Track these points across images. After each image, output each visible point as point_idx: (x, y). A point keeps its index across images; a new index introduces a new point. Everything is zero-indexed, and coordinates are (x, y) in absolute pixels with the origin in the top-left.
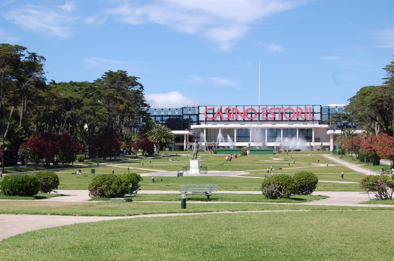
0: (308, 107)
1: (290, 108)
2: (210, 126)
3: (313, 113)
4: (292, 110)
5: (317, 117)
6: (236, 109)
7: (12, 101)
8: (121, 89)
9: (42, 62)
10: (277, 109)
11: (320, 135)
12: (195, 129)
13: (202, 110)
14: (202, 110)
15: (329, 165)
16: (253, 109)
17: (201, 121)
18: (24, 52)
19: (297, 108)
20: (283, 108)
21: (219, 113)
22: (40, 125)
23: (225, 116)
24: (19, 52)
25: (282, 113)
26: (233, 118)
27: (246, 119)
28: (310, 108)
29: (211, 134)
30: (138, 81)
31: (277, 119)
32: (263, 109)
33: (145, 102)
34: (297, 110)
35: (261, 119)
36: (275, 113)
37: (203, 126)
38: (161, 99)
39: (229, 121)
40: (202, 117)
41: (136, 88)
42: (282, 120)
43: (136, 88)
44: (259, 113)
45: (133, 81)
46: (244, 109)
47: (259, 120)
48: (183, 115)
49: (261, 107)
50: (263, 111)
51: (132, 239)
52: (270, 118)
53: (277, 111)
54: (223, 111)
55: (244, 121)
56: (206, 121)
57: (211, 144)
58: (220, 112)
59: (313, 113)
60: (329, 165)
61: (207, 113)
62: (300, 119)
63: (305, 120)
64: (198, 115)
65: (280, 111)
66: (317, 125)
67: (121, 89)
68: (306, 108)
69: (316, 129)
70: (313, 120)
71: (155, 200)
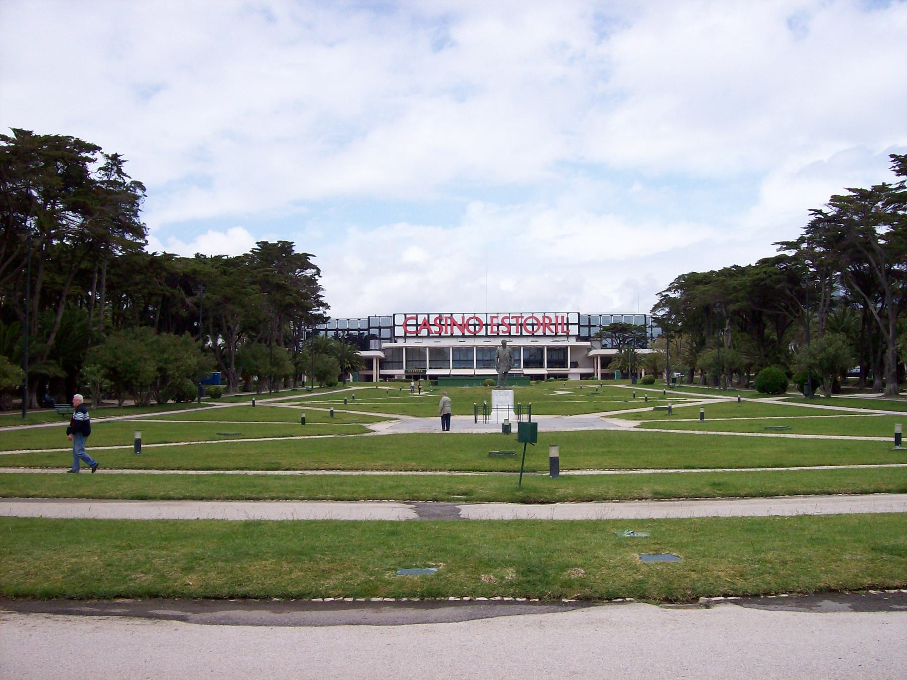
0: (560, 315)
1: (533, 317)
2: (411, 343)
3: (568, 324)
4: (537, 319)
5: (574, 330)
6: (451, 318)
7: (61, 203)
8: (277, 278)
9: (139, 192)
10: (513, 317)
11: (579, 358)
12: (388, 348)
13: (400, 320)
14: (400, 320)
15: (434, 424)
16: (478, 319)
17: (398, 337)
18: (98, 155)
19: (544, 317)
20: (522, 317)
21: (425, 325)
22: (111, 380)
23: (435, 329)
24: (84, 155)
25: (521, 325)
26: (446, 332)
27: (467, 334)
28: (563, 317)
29: (415, 354)
30: (312, 260)
31: (513, 333)
32: (492, 318)
33: (321, 299)
34: (544, 320)
35: (489, 334)
36: (510, 325)
37: (400, 343)
38: (348, 296)
39: (440, 336)
40: (399, 331)
41: (309, 272)
42: (522, 336)
43: (309, 272)
44: (487, 325)
45: (303, 261)
46: (463, 318)
47: (487, 336)
48: (369, 328)
49: (489, 315)
50: (492, 321)
51: (450, 574)
52: (503, 332)
53: (513, 321)
54: (432, 322)
55: (463, 336)
56: (405, 337)
57: (414, 371)
58: (426, 324)
59: (568, 324)
60: (434, 424)
61: (407, 325)
62: (548, 333)
63: (556, 335)
64: (392, 328)
65: (517, 321)
66: (573, 342)
67: (277, 278)
68: (557, 317)
69: (572, 347)
70: (568, 336)
71: (179, 469)
